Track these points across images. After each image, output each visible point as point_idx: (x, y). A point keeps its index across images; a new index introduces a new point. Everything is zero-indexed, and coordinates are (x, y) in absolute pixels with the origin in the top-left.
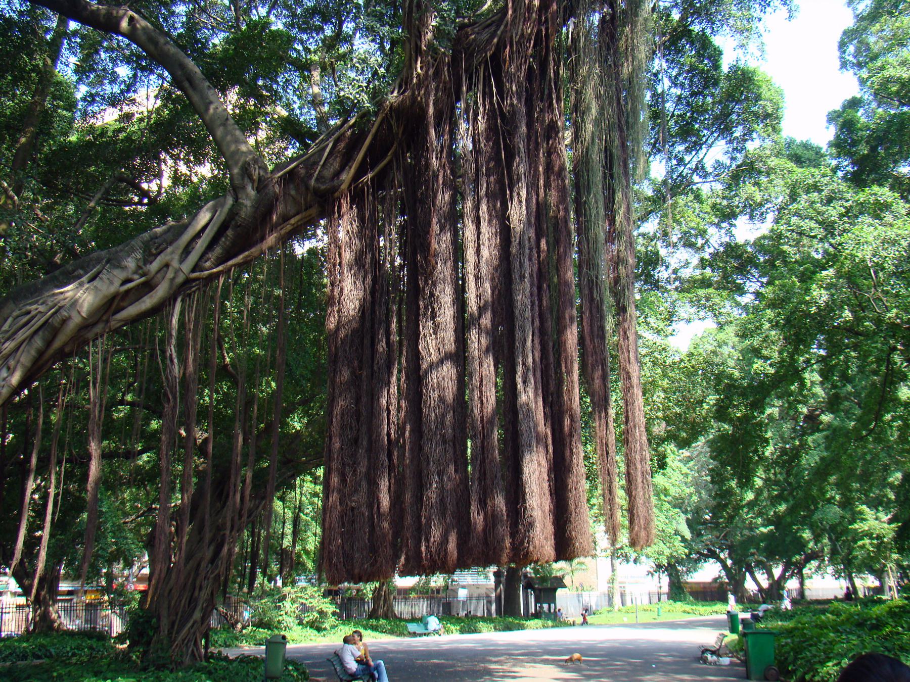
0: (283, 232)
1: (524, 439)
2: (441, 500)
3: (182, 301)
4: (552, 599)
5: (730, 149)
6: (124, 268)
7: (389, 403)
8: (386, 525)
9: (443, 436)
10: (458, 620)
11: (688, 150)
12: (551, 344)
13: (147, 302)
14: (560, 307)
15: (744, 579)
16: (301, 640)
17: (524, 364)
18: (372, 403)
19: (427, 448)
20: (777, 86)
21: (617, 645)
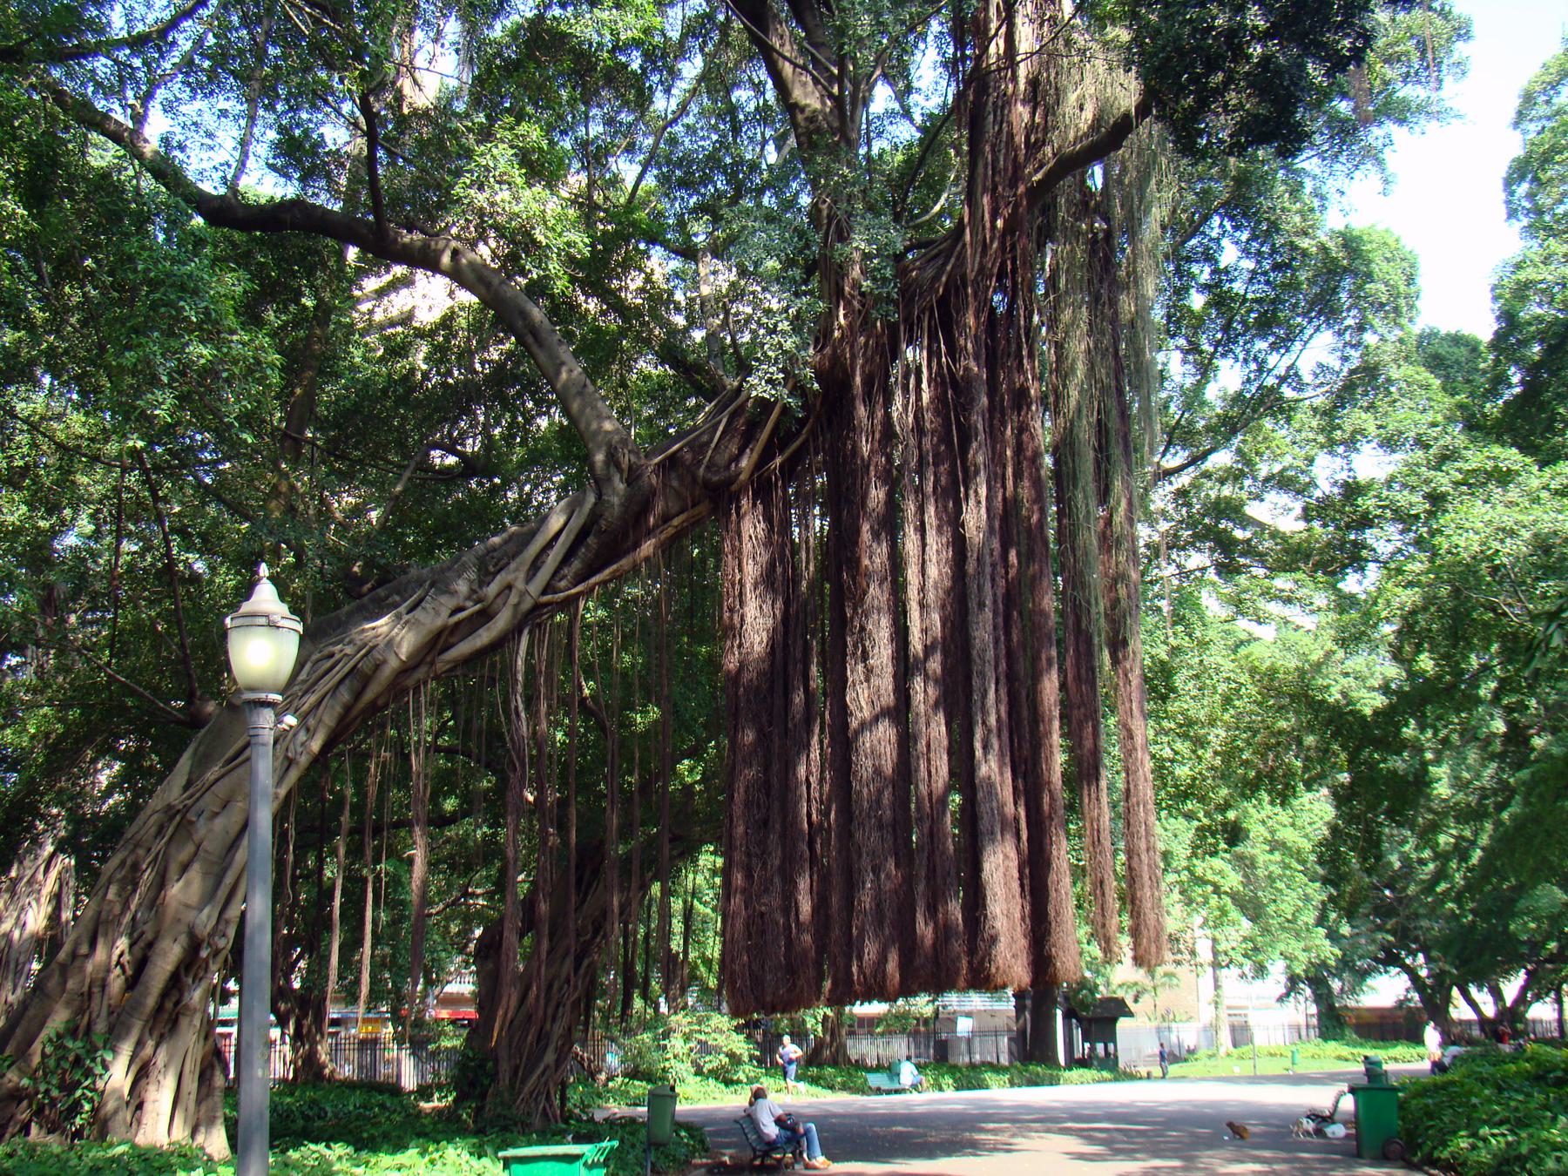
0: (663, 536)
1: (984, 824)
2: (878, 905)
3: (530, 633)
4: (1110, 1036)
5: (1340, 345)
6: (454, 593)
7: (809, 773)
8: (807, 938)
9: (880, 819)
10: (953, 1069)
11: (1274, 347)
12: (1024, 693)
13: (484, 637)
14: (1041, 642)
15: (1448, 999)
16: (699, 1098)
17: (984, 723)
18: (787, 773)
19: (858, 835)
20: (1408, 249)
21: (1188, 1108)
